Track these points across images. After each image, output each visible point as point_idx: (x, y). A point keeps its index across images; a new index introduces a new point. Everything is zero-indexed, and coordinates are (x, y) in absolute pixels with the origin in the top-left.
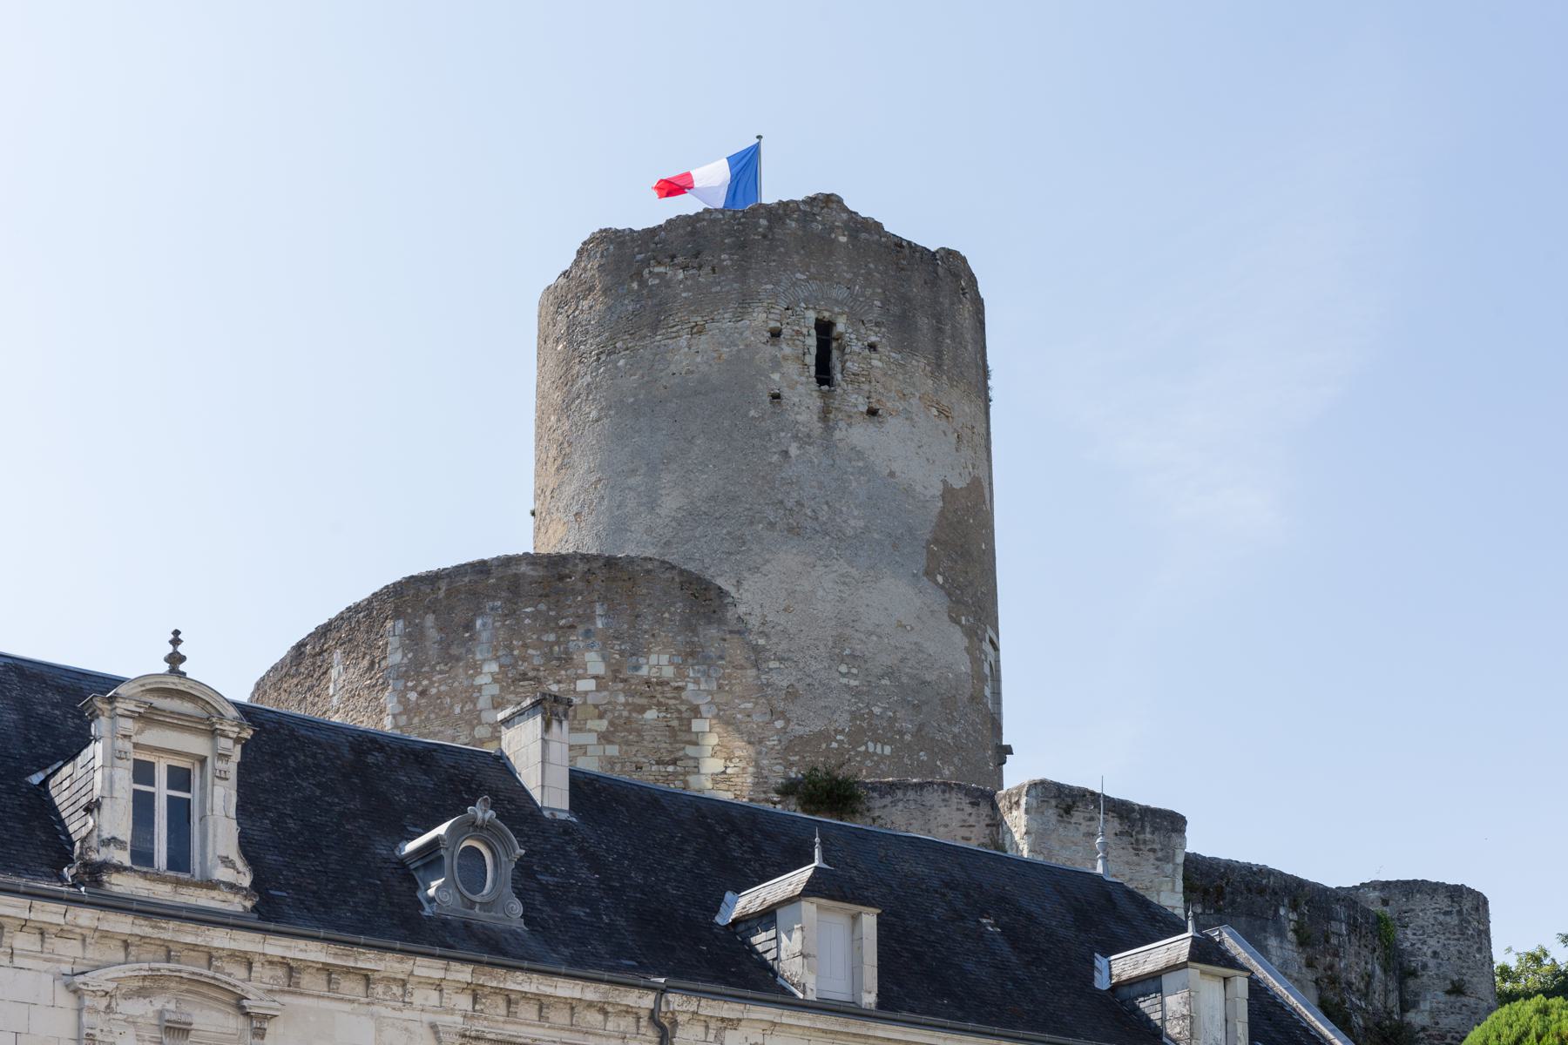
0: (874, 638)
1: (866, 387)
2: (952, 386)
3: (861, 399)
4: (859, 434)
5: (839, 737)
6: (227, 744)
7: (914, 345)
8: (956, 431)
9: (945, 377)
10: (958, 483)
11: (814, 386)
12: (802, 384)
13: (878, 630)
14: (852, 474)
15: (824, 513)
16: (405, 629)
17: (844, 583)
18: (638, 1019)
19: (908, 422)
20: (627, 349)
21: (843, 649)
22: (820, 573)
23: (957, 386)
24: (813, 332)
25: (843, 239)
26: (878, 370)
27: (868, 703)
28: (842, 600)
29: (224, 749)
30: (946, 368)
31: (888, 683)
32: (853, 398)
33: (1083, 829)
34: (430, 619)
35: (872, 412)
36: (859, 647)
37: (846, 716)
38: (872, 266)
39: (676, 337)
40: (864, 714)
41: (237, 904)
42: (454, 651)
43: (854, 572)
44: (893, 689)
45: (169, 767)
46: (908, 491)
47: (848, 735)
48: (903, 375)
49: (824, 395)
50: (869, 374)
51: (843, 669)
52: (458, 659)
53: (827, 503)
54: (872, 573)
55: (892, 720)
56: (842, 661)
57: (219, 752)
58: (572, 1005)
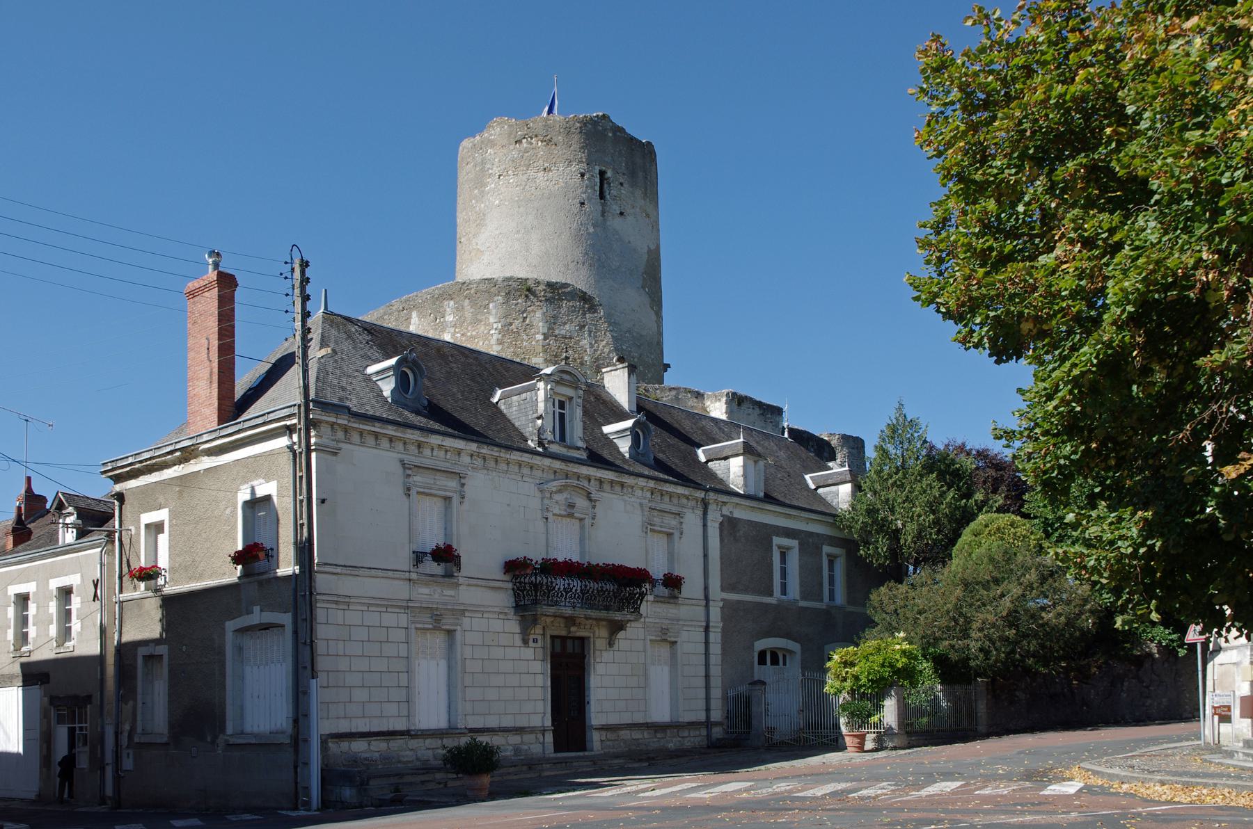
1: (619, 202)
4: (616, 223)
6: (581, 392)
10: (653, 247)
11: (599, 200)
18: (697, 502)
33: (746, 412)
34: (467, 302)
35: (621, 214)
42: (479, 317)
52: (481, 321)
58: (679, 496)
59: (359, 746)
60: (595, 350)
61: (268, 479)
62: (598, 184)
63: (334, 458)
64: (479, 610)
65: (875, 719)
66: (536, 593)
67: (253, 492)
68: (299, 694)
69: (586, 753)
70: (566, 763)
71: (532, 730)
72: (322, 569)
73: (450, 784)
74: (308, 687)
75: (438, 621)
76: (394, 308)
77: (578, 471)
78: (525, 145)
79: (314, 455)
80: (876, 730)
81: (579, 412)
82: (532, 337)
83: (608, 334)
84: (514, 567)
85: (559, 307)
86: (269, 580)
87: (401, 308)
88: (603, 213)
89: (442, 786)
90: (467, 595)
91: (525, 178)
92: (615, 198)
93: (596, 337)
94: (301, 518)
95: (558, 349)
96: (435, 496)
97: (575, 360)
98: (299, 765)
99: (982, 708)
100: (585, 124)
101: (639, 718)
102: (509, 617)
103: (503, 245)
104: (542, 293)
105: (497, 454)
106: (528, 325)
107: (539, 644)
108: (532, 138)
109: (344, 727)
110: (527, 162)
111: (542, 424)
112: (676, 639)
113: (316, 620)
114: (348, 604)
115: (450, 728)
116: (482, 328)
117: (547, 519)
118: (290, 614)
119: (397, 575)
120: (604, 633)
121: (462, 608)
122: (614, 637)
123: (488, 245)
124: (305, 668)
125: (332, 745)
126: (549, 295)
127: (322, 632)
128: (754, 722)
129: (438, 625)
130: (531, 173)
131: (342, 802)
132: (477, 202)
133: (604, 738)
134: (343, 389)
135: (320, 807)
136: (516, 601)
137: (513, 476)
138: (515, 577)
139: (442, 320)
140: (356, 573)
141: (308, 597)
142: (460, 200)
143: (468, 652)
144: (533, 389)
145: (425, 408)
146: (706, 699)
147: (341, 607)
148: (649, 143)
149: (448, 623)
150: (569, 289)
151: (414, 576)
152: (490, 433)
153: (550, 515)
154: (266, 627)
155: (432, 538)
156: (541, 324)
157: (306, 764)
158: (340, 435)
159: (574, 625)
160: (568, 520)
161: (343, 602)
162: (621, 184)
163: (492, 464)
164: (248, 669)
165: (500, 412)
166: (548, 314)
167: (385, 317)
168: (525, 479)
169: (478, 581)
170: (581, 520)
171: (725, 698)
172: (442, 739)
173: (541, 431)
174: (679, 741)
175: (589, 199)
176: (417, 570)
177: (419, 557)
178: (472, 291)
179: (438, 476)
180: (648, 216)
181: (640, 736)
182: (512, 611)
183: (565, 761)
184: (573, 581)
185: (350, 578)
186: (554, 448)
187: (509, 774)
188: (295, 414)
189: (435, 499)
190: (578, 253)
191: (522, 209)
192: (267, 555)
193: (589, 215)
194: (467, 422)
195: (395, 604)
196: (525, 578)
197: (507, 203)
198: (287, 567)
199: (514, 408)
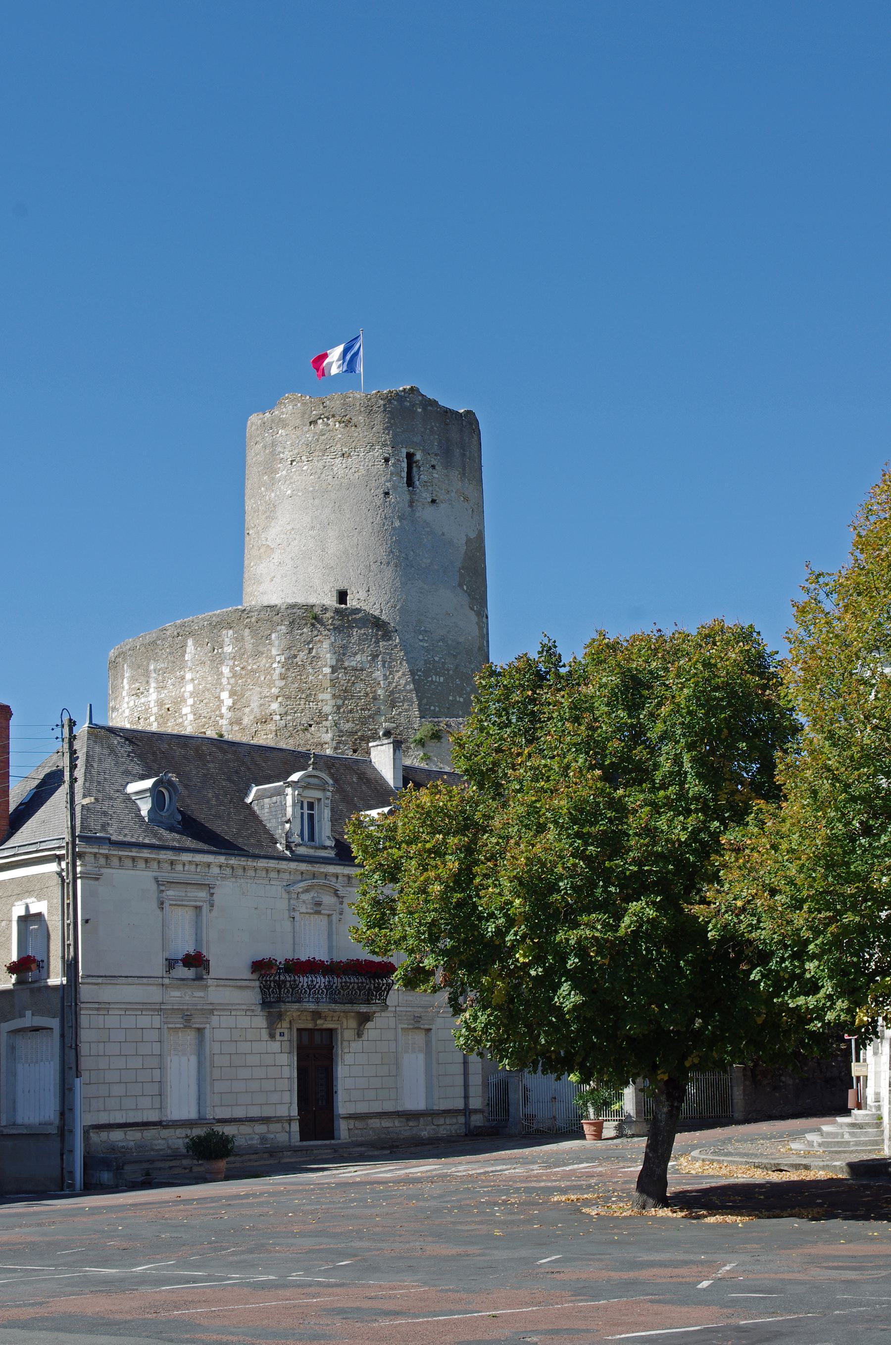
0: (435, 621)
1: (430, 488)
3: (428, 495)
4: (426, 513)
5: (419, 673)
10: (472, 535)
11: (406, 488)
17: (421, 592)
24: (405, 460)
28: (420, 601)
34: (247, 631)
37: (422, 662)
38: (433, 424)
41: (331, 854)
42: (261, 649)
47: (423, 672)
49: (411, 493)
51: (421, 637)
53: (413, 550)
54: (434, 587)
55: (444, 664)
56: (420, 633)
59: (116, 1136)
61: (39, 898)
62: (406, 470)
63: (97, 882)
64: (228, 1008)
65: (615, 1107)
66: (280, 991)
67: (27, 908)
68: (66, 1091)
69: (333, 1142)
70: (307, 1150)
71: (278, 1120)
72: (86, 981)
73: (195, 1169)
74: (73, 1085)
75: (188, 1021)
76: (168, 633)
77: (325, 871)
78: (321, 427)
79: (79, 882)
80: (618, 1118)
81: (327, 813)
82: (319, 670)
83: (404, 663)
84: (260, 967)
86: (39, 989)
87: (175, 633)
88: (411, 503)
89: (187, 1171)
90: (216, 994)
91: (320, 464)
92: (425, 484)
94: (68, 939)
95: (348, 683)
96: (186, 906)
97: (367, 694)
98: (65, 1152)
99: (738, 1094)
100: (390, 401)
101: (389, 1107)
102: (256, 1013)
104: (330, 621)
105: (244, 863)
106: (314, 657)
107: (286, 1038)
108: (328, 419)
109: (103, 1119)
111: (290, 828)
112: (430, 1027)
113: (80, 1026)
114: (108, 1009)
115: (200, 1119)
117: (294, 918)
118: (58, 1019)
119: (151, 981)
120: (353, 1023)
121: (211, 1007)
122: (362, 1027)
123: (278, 541)
124: (71, 1068)
125: (94, 1137)
126: (337, 623)
127: (85, 1035)
128: (512, 1110)
129: (188, 1024)
130: (327, 459)
131: (101, 1185)
133: (351, 1127)
134: (105, 814)
135: (82, 1188)
136: (263, 998)
137: (261, 881)
138: (262, 976)
139: (220, 650)
140: (115, 982)
141: (73, 1007)
142: (248, 484)
143: (216, 1048)
144: (280, 792)
145: (179, 823)
146: (464, 1086)
147: (101, 1013)
148: (469, 413)
149: (197, 1022)
150: (360, 615)
151: (166, 981)
152: (240, 842)
153: (297, 915)
154: (36, 1029)
155: (185, 946)
156: (328, 655)
157: (71, 1151)
158: (102, 861)
159: (320, 1018)
160: (316, 916)
161: (103, 1007)
162: (433, 467)
163: (240, 872)
164: (20, 1067)
165: (253, 814)
166: (337, 644)
167: (159, 642)
168: (272, 882)
169: (226, 981)
170: (329, 915)
171: (486, 1084)
172: (191, 1128)
174: (434, 1129)
175: (395, 488)
176: (170, 976)
177: (171, 964)
178: (253, 620)
179: (189, 889)
180: (466, 499)
181: (391, 1125)
182: (259, 1008)
183: (307, 1149)
184: (316, 977)
185: (110, 986)
186: (302, 850)
187: (250, 1160)
188: (63, 847)
189: (187, 908)
190: (382, 553)
191: (317, 501)
192: (38, 966)
194: (218, 832)
195: (149, 1007)
196: (271, 977)
197: (300, 494)
198: (56, 979)
199: (266, 810)
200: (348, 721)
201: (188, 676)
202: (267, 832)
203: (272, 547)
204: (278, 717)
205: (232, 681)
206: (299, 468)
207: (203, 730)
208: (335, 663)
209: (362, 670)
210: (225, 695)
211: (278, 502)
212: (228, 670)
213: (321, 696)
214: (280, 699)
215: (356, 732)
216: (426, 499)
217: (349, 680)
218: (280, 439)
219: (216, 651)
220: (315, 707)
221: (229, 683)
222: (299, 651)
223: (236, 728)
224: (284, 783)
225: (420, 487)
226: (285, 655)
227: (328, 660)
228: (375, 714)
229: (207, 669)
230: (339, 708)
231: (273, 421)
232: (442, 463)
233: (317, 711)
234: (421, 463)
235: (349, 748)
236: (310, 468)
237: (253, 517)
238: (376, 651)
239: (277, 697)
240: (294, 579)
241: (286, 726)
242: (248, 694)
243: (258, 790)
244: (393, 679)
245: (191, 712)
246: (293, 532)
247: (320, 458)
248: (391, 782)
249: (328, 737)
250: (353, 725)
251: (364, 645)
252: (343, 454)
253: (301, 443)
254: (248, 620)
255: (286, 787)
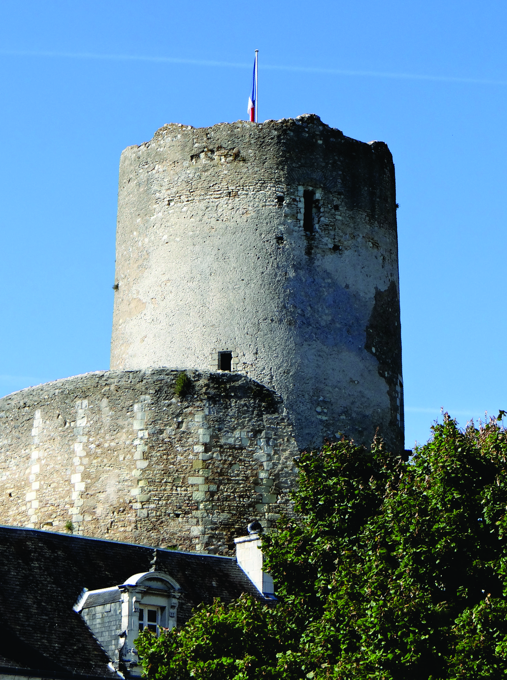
0: (337, 389)
1: (332, 233)
2: (380, 227)
3: (330, 240)
7: (360, 205)
8: (382, 255)
9: (376, 222)
10: (383, 288)
12: (296, 232)
13: (339, 385)
14: (325, 287)
15: (308, 312)
16: (89, 406)
17: (320, 356)
19: (356, 253)
20: (188, 201)
21: (319, 397)
22: (306, 350)
23: (383, 227)
24: (302, 199)
25: (320, 142)
26: (339, 222)
27: (333, 431)
28: (318, 366)
29: (174, 603)
30: (377, 216)
31: (345, 418)
32: (325, 240)
34: (105, 401)
35: (336, 248)
36: (328, 395)
38: (336, 158)
39: (219, 198)
40: (330, 438)
42: (120, 422)
43: (325, 348)
44: (347, 421)
45: (149, 610)
46: (356, 296)
48: (353, 224)
50: (334, 225)
51: (319, 409)
52: (122, 428)
53: (310, 305)
54: (336, 349)
56: (318, 405)
57: (172, 605)
60: (274, 464)
83: (293, 441)
85: (226, 408)
87: (22, 404)
88: (309, 251)
91: (202, 205)
92: (326, 227)
93: (276, 445)
95: (224, 464)
97: (247, 478)
100: (285, 132)
103: (172, 296)
104: (204, 390)
106: (184, 432)
108: (212, 152)
110: (205, 184)
111: (125, 643)
116: (123, 437)
123: (152, 295)
126: (212, 391)
132: (140, 234)
139: (72, 424)
144: (115, 599)
150: (240, 382)
156: (201, 431)
166: (211, 417)
173: (124, 652)
175: (290, 232)
178: (113, 387)
180: (376, 245)
190: (273, 308)
191: (198, 248)
193: (289, 254)
199: (98, 621)
200: (223, 511)
201: (35, 454)
202: (98, 647)
203: (144, 301)
204: (138, 505)
205: (86, 461)
206: (177, 210)
207: (50, 521)
208: (208, 441)
209: (241, 448)
210: (76, 478)
211: (152, 249)
212: (81, 448)
213: (191, 480)
214: (142, 483)
215: (233, 525)
216: (326, 244)
217: (225, 460)
218: (157, 176)
219: (68, 425)
220: (183, 493)
221: (81, 464)
222: (166, 425)
223: (88, 518)
224: (120, 587)
225: (319, 230)
226: (150, 431)
227: (201, 436)
228: (257, 503)
229: (56, 445)
230: (212, 494)
231: (148, 155)
232: (346, 204)
233: (186, 498)
234: (321, 203)
235: (224, 544)
236: (191, 209)
237: (123, 266)
238: (259, 426)
239: (139, 481)
240: (169, 339)
241: (148, 516)
242: (103, 477)
243: (90, 596)
244: (279, 459)
245: (37, 499)
246: (168, 284)
247: (202, 197)
248: (259, 586)
249: (196, 531)
250: (229, 516)
251: (244, 418)
252: (230, 193)
253: (180, 180)
254: (107, 388)
255: (122, 592)
